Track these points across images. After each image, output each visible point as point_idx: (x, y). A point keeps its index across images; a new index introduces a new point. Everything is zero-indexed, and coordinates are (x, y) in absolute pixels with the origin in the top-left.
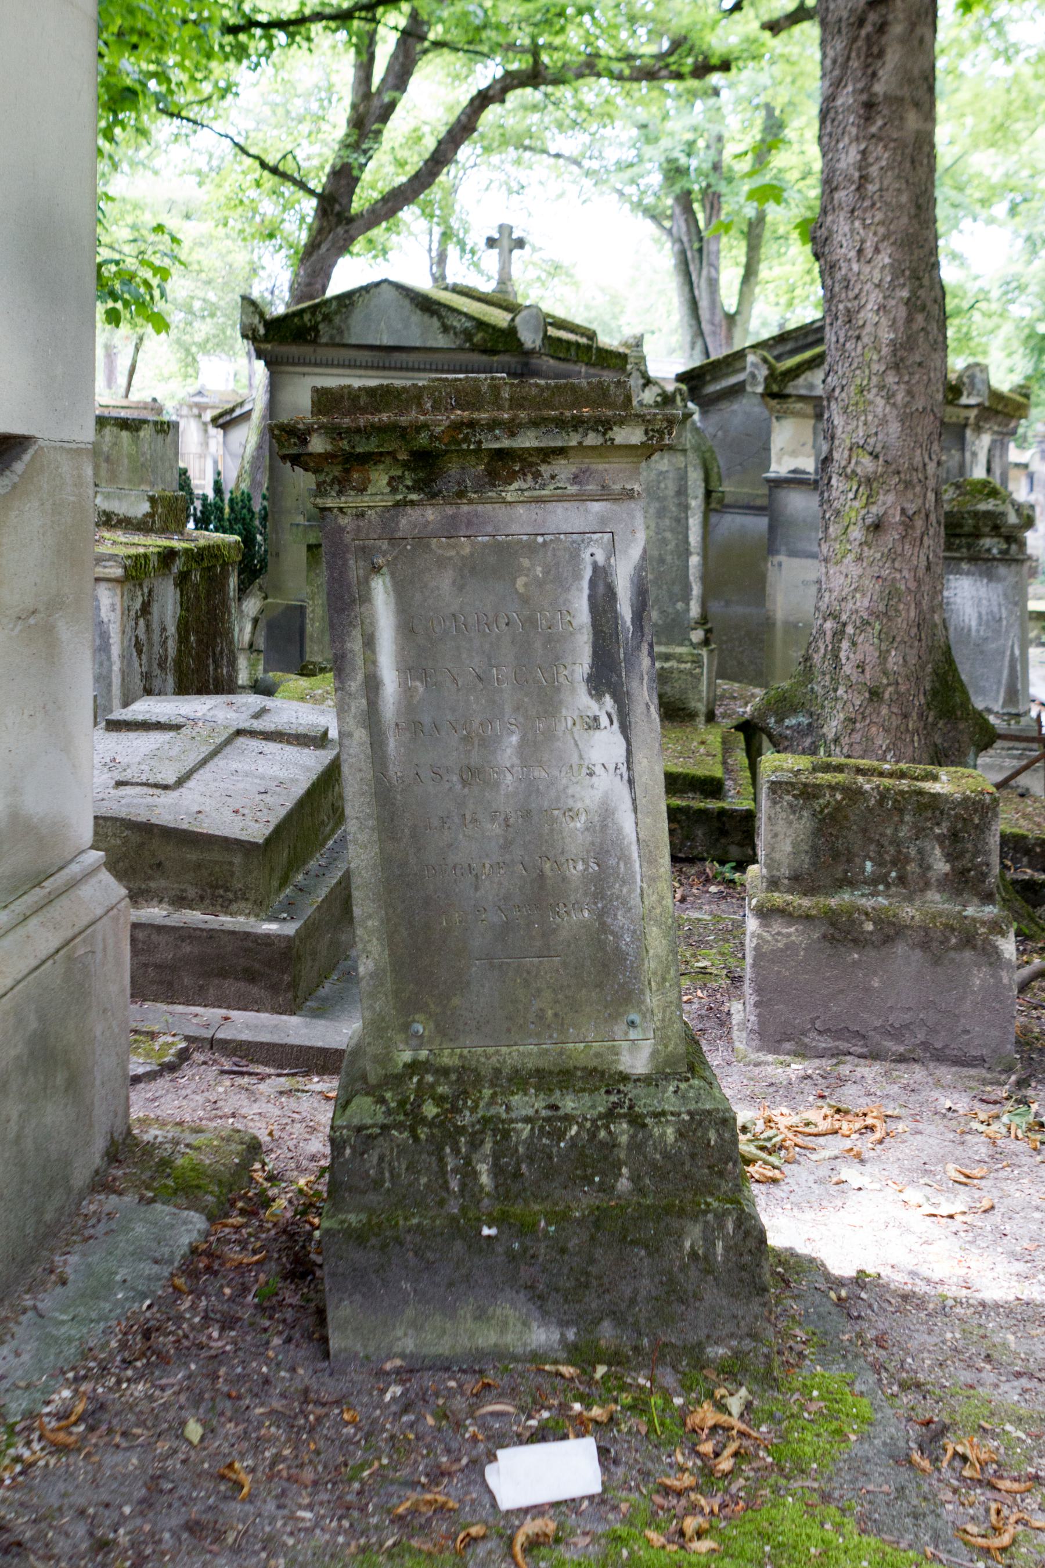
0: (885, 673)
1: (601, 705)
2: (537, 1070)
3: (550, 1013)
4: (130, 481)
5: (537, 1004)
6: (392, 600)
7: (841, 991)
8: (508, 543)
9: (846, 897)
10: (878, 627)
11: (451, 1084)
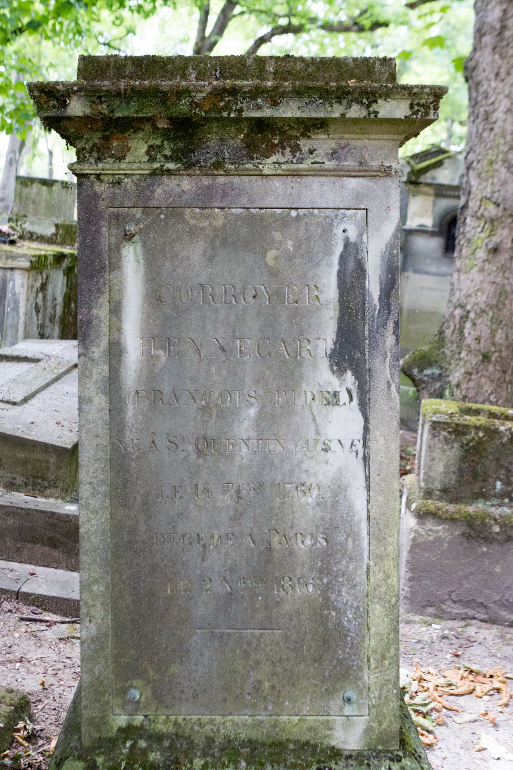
0: (494, 344)
1: (342, 381)
2: (250, 741)
3: (267, 684)
4: (45, 215)
5: (254, 676)
6: (142, 268)
7: (472, 574)
8: (262, 217)
9: (480, 505)
10: (491, 314)
11: (163, 751)
